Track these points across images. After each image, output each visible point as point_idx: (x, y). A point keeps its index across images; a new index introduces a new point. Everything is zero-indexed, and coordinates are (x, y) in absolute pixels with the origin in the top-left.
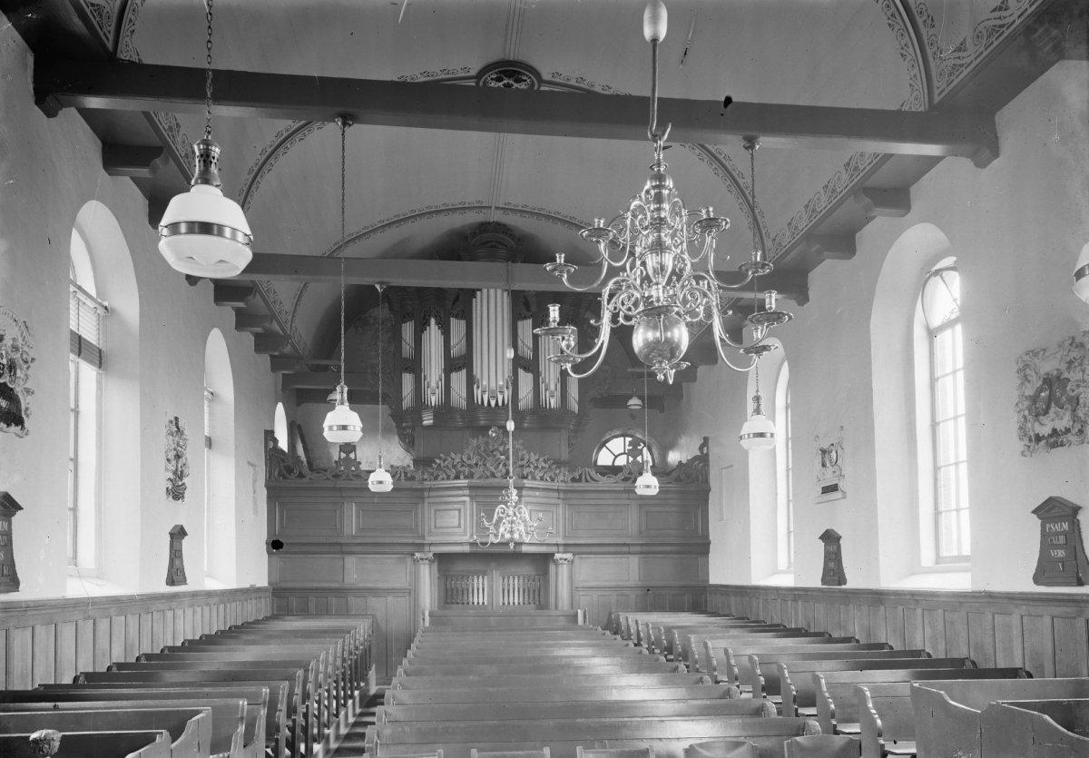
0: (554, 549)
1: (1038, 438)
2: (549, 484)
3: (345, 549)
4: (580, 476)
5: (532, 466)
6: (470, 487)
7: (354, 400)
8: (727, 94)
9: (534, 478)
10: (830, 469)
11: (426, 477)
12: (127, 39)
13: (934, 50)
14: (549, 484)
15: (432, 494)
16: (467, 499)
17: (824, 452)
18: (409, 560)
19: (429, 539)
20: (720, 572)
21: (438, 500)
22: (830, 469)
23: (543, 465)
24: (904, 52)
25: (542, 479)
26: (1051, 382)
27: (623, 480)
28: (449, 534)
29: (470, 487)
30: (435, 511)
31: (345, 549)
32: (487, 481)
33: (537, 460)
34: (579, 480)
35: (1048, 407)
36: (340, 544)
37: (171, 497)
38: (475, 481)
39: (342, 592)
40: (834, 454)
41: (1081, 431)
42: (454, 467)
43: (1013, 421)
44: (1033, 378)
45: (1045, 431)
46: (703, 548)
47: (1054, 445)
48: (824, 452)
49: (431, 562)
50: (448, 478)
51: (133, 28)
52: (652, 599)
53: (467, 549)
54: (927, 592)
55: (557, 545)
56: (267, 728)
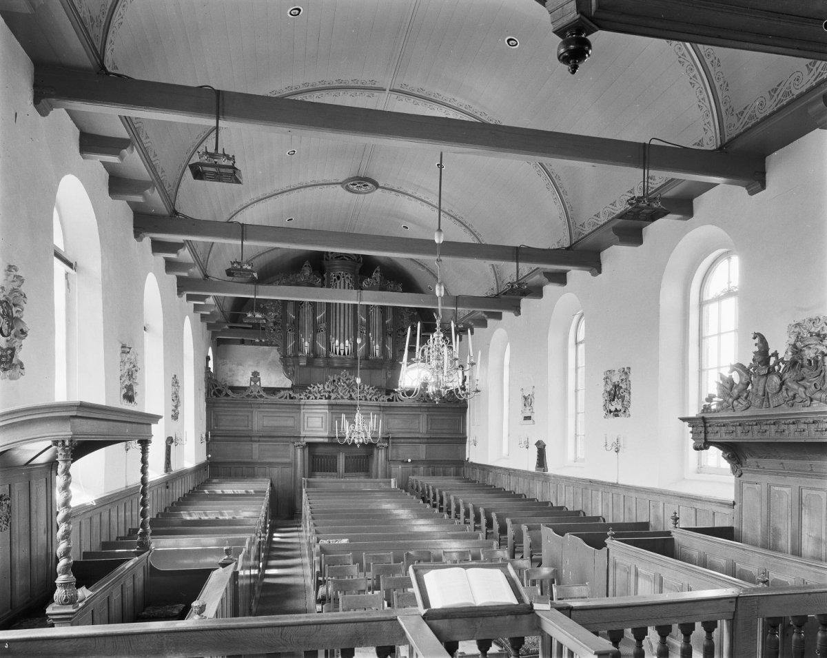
1: (611, 412)
2: (375, 403)
3: (253, 439)
4: (393, 398)
6: (329, 405)
7: (77, 596)
9: (366, 400)
10: (528, 408)
11: (302, 397)
13: (711, 60)
14: (375, 403)
15: (306, 407)
16: (327, 411)
17: (526, 398)
18: (291, 445)
19: (303, 434)
20: (474, 454)
21: (310, 411)
22: (528, 408)
25: (371, 399)
26: (616, 386)
28: (318, 431)
29: (329, 405)
31: (253, 439)
33: (368, 389)
34: (392, 400)
35: (614, 397)
36: (251, 437)
37: (230, 266)
38: (332, 401)
39: (251, 464)
40: (530, 400)
41: (625, 411)
42: (320, 392)
43: (602, 402)
44: (609, 382)
45: (613, 409)
46: (462, 440)
47: (617, 416)
48: (526, 398)
49: (304, 448)
50: (316, 398)
51: (121, 20)
52: (434, 466)
53: (326, 440)
56: (123, 622)
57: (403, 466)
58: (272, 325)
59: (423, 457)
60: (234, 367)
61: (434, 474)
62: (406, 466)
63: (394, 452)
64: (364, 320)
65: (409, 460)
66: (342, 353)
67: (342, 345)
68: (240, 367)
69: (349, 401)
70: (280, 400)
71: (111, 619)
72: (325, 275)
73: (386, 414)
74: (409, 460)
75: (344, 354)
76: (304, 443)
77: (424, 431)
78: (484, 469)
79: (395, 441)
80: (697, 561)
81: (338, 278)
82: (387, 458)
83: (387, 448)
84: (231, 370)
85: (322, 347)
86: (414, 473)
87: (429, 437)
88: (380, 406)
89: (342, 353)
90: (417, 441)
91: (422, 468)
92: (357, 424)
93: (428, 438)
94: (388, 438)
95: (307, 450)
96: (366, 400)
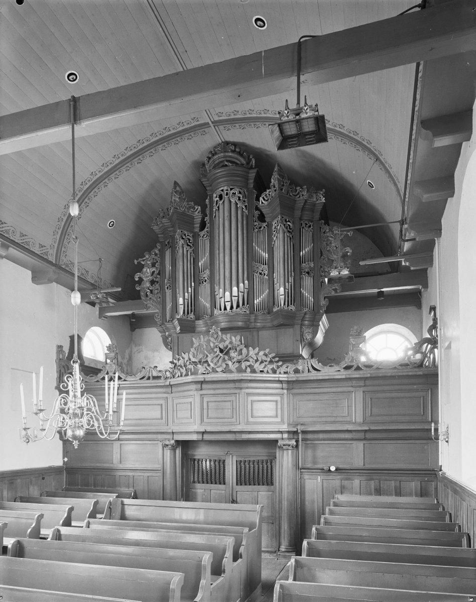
0: (278, 436)
5: (251, 360)
8: (72, 95)
12: (199, 133)
14: (271, 376)
16: (285, 391)
23: (264, 358)
24: (242, 128)
27: (344, 368)
30: (276, 401)
32: (209, 376)
38: (200, 378)
49: (174, 448)
54: (79, 521)
55: (281, 432)
57: (326, 477)
58: (148, 285)
59: (358, 462)
60: (150, 354)
61: (378, 492)
62: (331, 477)
63: (309, 453)
64: (265, 255)
65: (333, 468)
66: (228, 308)
67: (227, 294)
68: (156, 354)
69: (224, 375)
70: (142, 381)
71: (297, 577)
72: (207, 200)
73: (294, 394)
74: (333, 468)
75: (225, 309)
76: (172, 442)
77: (360, 419)
78: (455, 492)
79: (310, 436)
80: (426, 197)
81: (221, 197)
82: (297, 466)
83: (297, 446)
84: (146, 358)
85: (205, 302)
86: (343, 490)
87: (367, 428)
88: (281, 382)
89: (228, 308)
90: (347, 436)
91: (356, 482)
92: (71, 393)
93: (365, 431)
94: (296, 433)
95: (178, 452)
96: (253, 371)
